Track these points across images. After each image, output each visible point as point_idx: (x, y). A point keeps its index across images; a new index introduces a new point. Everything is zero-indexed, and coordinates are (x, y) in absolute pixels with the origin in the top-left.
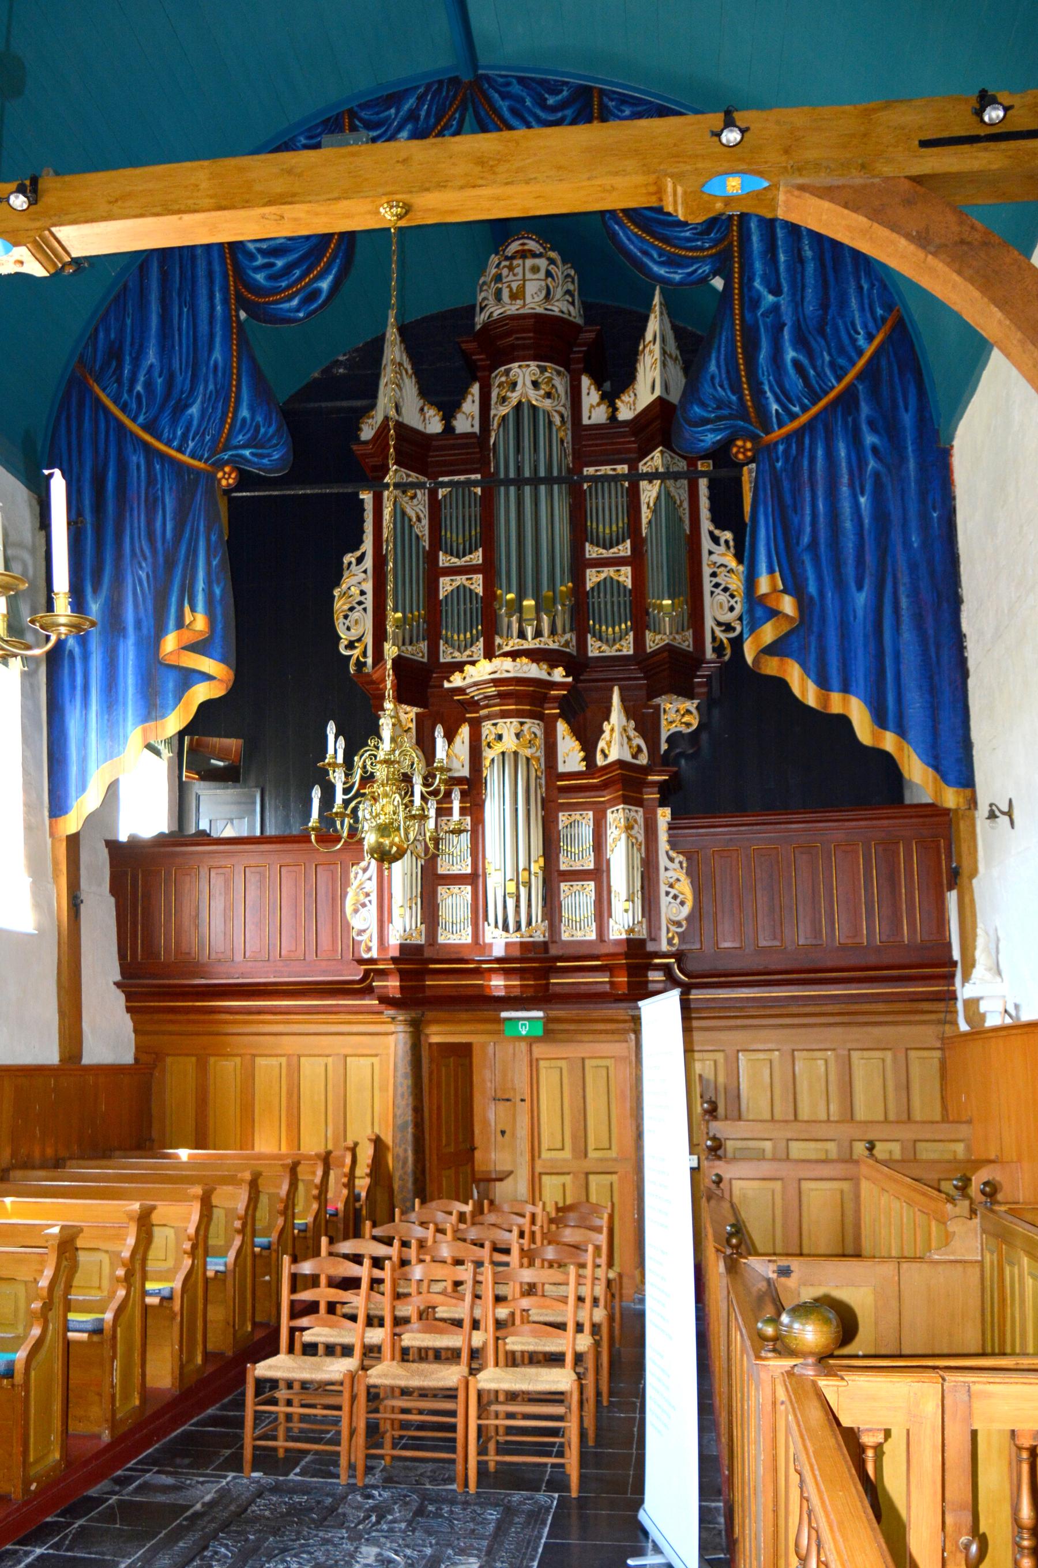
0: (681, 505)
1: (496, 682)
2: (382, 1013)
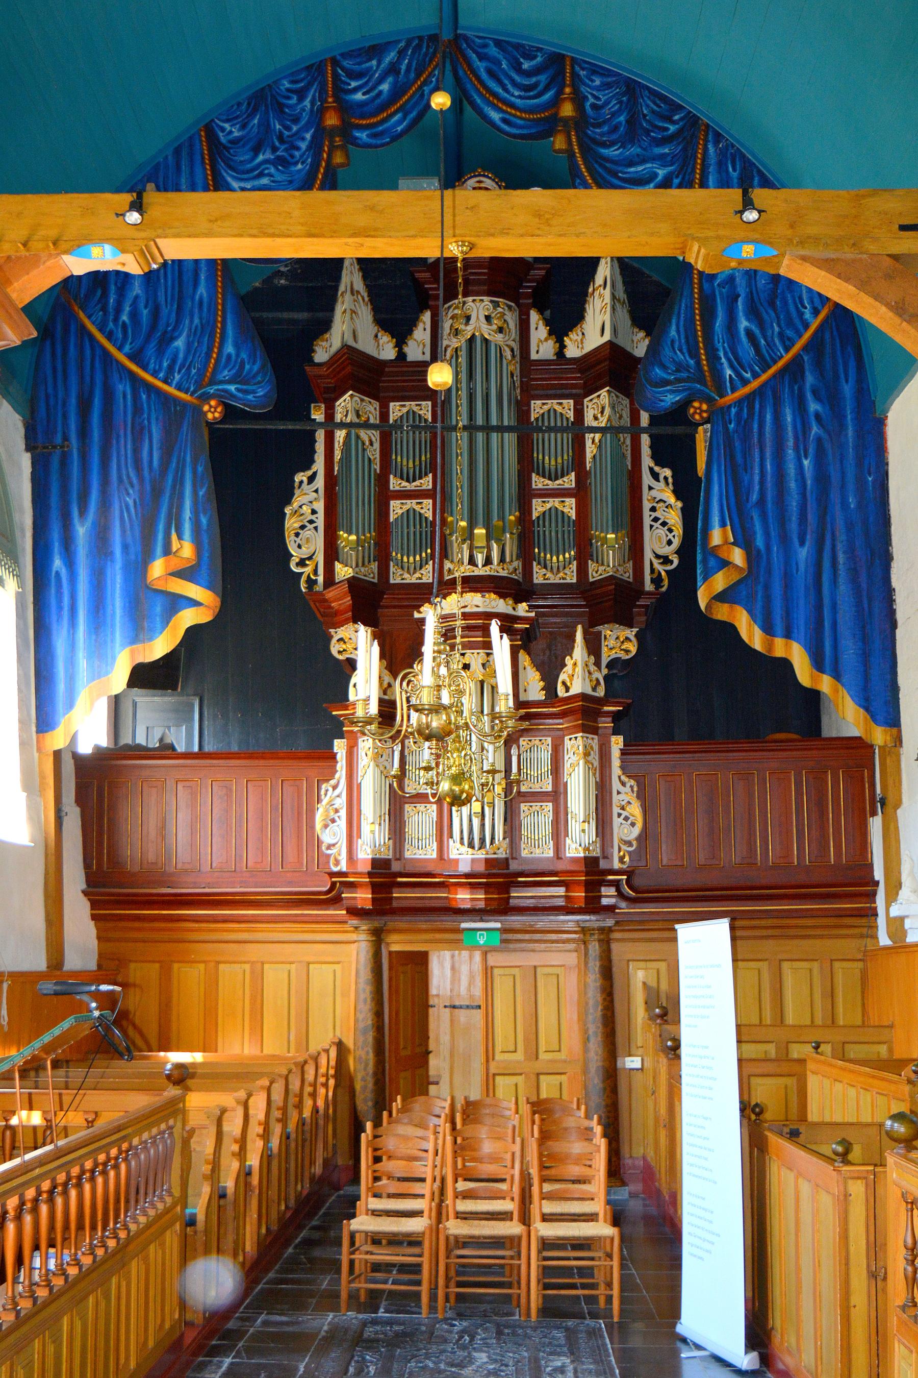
0: (624, 442)
2: (346, 922)
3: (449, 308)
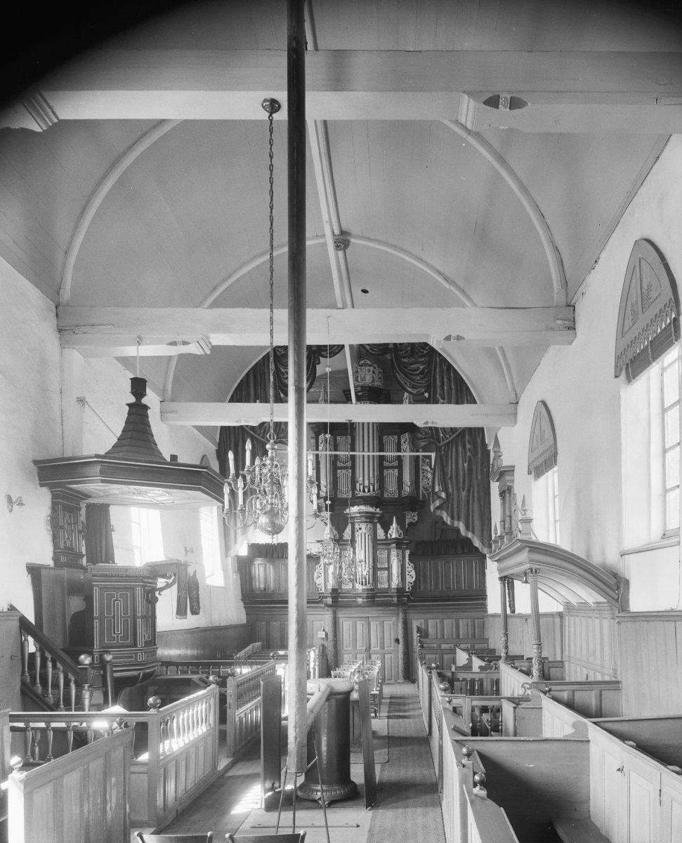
1: (360, 513)
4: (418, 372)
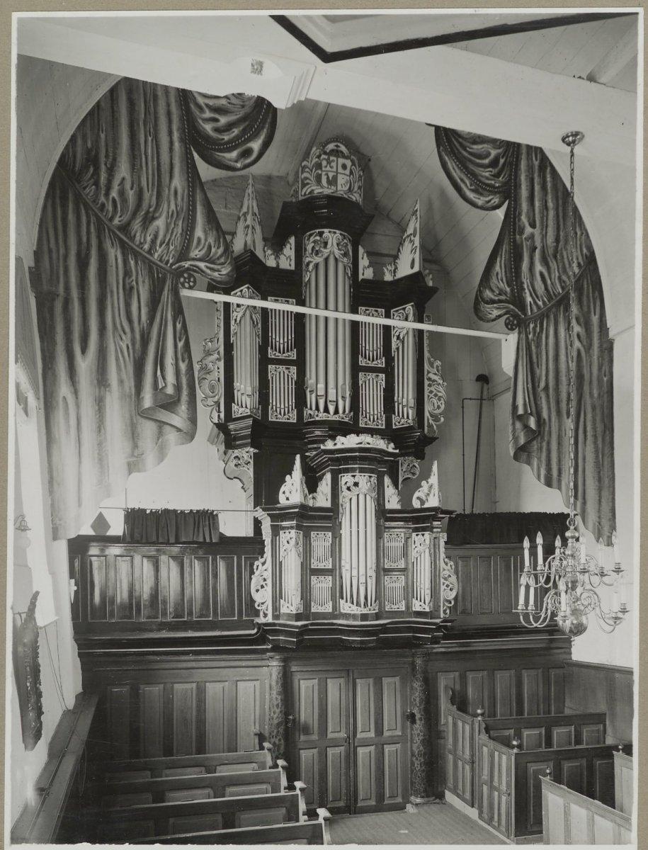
3: (311, 235)
4: (486, 161)
